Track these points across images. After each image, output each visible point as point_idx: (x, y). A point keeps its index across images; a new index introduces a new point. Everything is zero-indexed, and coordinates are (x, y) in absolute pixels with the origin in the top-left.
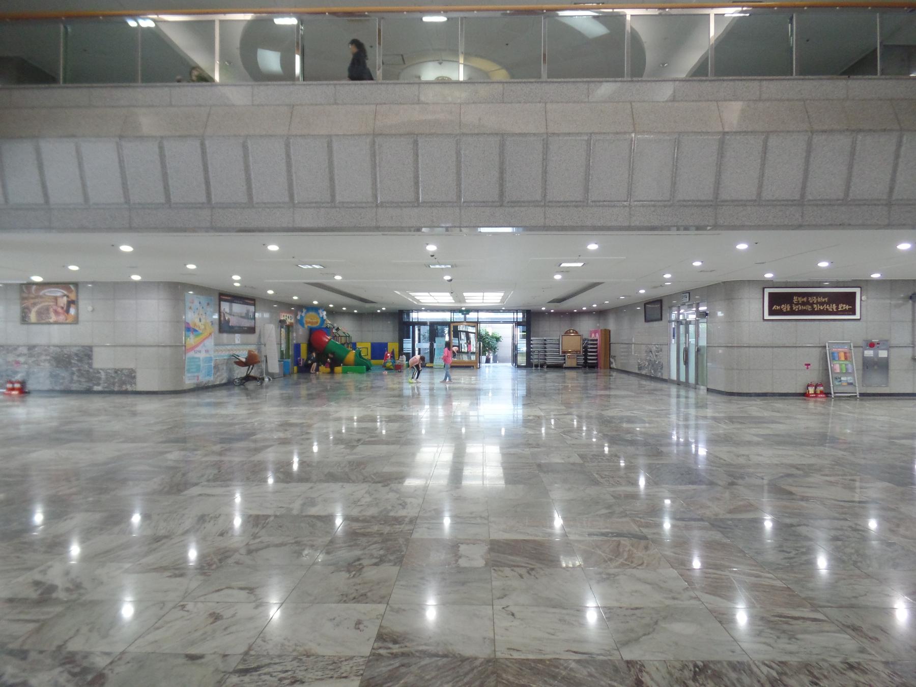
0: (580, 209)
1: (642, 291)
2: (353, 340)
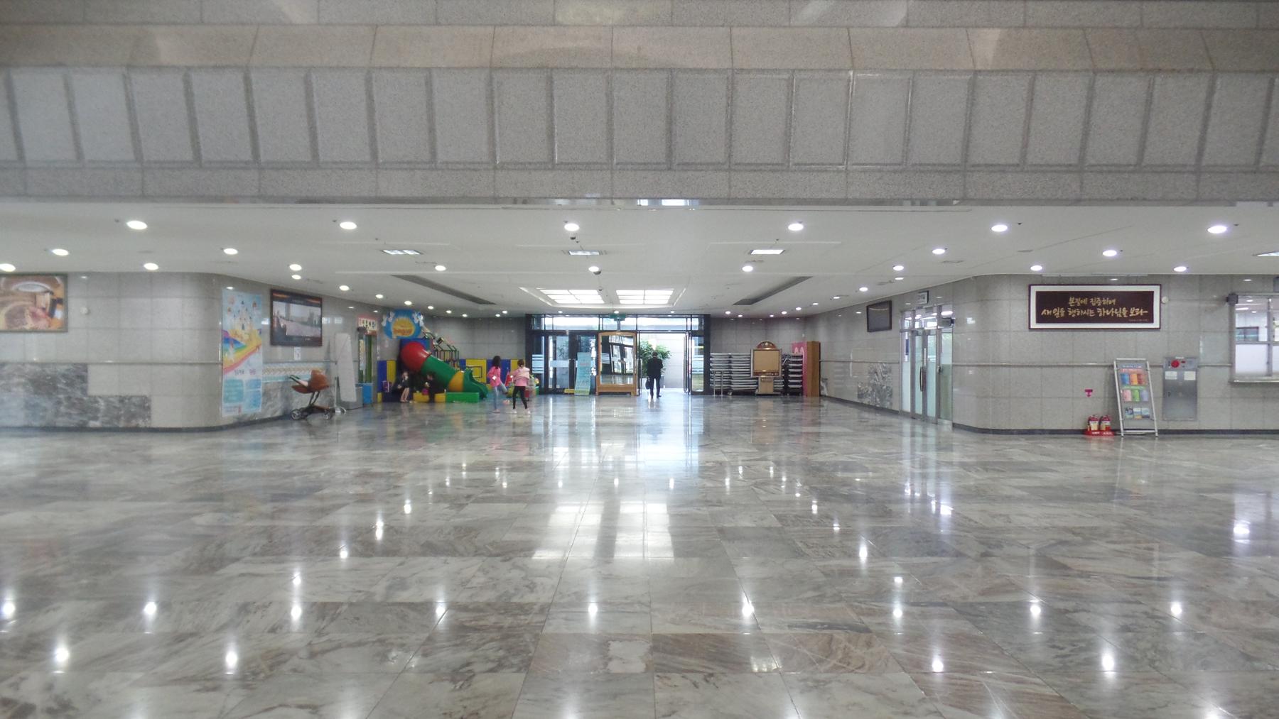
0: (778, 175)
1: (864, 289)
2: (462, 356)
